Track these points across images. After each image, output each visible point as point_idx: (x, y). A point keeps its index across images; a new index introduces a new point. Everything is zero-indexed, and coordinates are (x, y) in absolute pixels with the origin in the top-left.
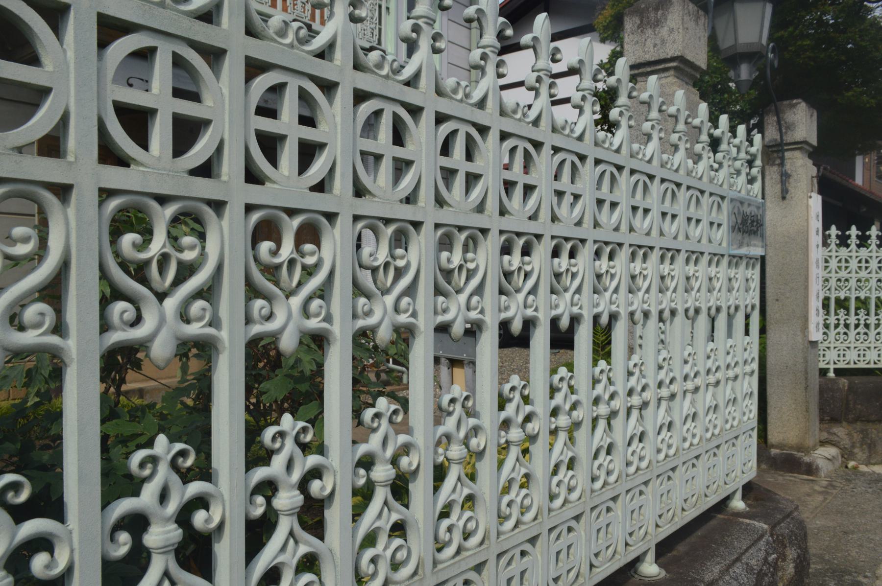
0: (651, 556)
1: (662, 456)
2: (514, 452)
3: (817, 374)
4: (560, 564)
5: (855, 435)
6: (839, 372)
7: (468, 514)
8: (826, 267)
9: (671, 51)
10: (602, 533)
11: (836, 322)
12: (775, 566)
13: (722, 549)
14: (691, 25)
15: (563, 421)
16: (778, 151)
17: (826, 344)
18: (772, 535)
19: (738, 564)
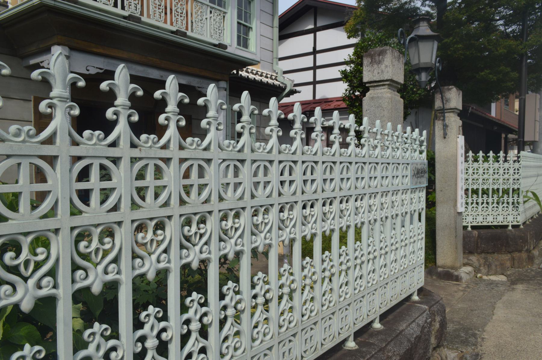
0: (377, 320)
1: (382, 278)
2: (327, 280)
3: (462, 229)
4: (307, 345)
5: (481, 260)
6: (473, 227)
7: (312, 304)
8: (467, 173)
9: (386, 76)
10: (358, 311)
12: (430, 324)
13: (407, 317)
14: (396, 63)
15: (344, 267)
16: (442, 113)
17: (467, 213)
18: (429, 311)
19: (414, 323)
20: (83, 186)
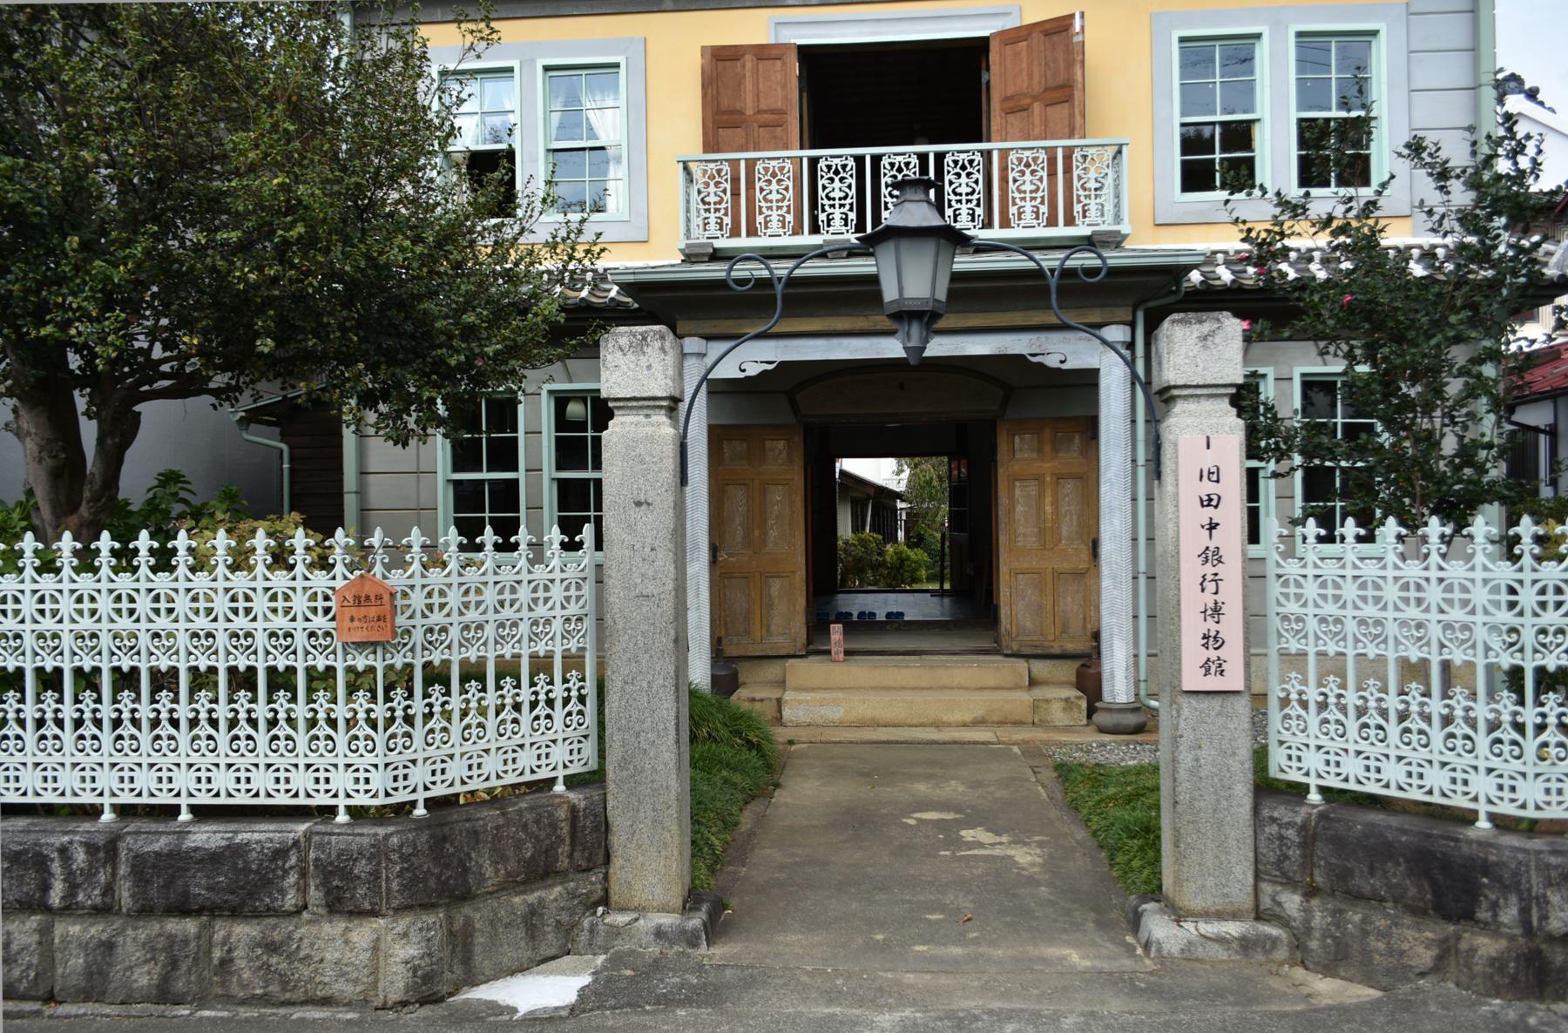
11: (1321, 699)
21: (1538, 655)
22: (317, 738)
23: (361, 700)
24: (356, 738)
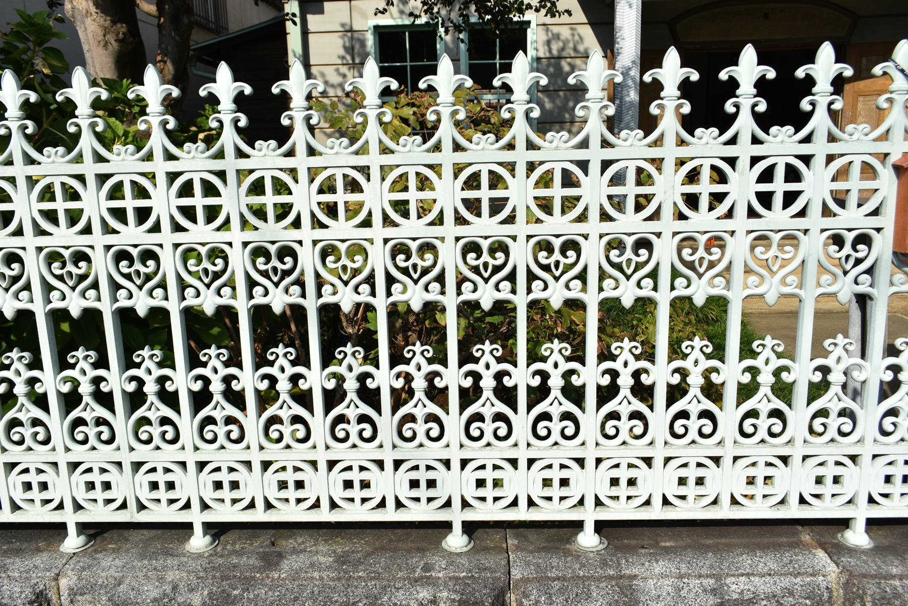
11: (818, 377)
20: (765, 187)
21: (753, 279)
22: (148, 421)
23: (351, 360)
24: (210, 420)
